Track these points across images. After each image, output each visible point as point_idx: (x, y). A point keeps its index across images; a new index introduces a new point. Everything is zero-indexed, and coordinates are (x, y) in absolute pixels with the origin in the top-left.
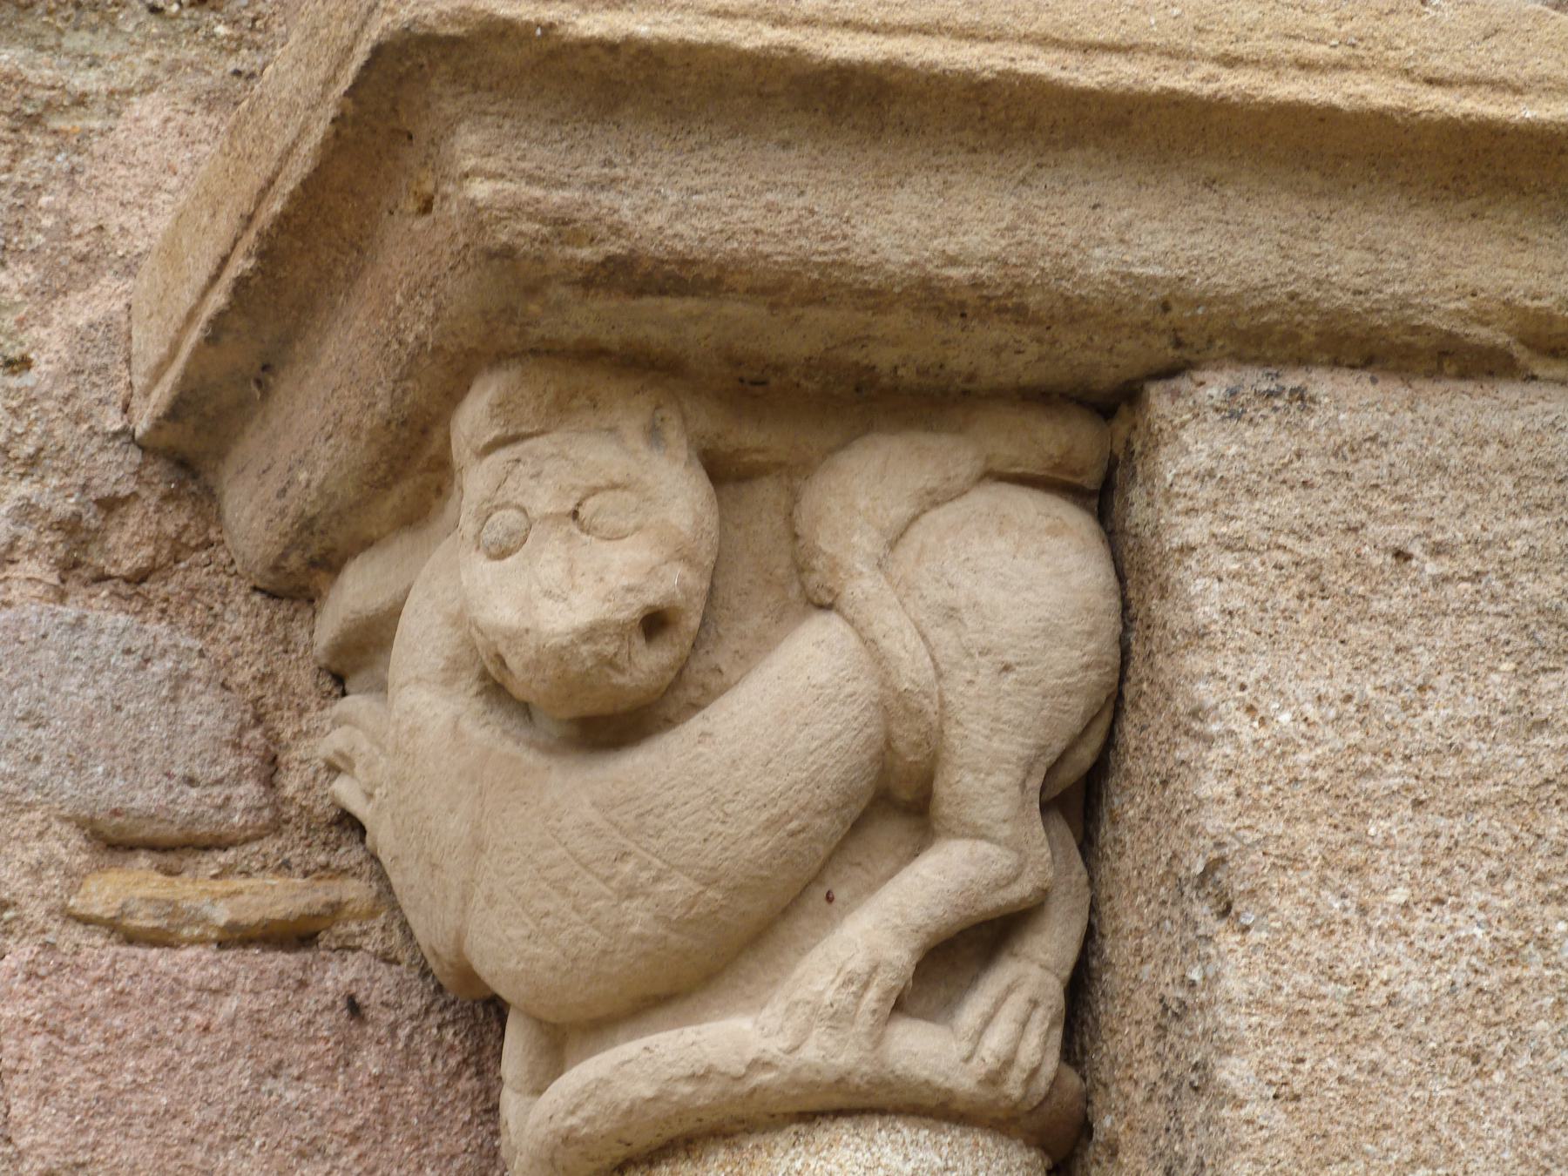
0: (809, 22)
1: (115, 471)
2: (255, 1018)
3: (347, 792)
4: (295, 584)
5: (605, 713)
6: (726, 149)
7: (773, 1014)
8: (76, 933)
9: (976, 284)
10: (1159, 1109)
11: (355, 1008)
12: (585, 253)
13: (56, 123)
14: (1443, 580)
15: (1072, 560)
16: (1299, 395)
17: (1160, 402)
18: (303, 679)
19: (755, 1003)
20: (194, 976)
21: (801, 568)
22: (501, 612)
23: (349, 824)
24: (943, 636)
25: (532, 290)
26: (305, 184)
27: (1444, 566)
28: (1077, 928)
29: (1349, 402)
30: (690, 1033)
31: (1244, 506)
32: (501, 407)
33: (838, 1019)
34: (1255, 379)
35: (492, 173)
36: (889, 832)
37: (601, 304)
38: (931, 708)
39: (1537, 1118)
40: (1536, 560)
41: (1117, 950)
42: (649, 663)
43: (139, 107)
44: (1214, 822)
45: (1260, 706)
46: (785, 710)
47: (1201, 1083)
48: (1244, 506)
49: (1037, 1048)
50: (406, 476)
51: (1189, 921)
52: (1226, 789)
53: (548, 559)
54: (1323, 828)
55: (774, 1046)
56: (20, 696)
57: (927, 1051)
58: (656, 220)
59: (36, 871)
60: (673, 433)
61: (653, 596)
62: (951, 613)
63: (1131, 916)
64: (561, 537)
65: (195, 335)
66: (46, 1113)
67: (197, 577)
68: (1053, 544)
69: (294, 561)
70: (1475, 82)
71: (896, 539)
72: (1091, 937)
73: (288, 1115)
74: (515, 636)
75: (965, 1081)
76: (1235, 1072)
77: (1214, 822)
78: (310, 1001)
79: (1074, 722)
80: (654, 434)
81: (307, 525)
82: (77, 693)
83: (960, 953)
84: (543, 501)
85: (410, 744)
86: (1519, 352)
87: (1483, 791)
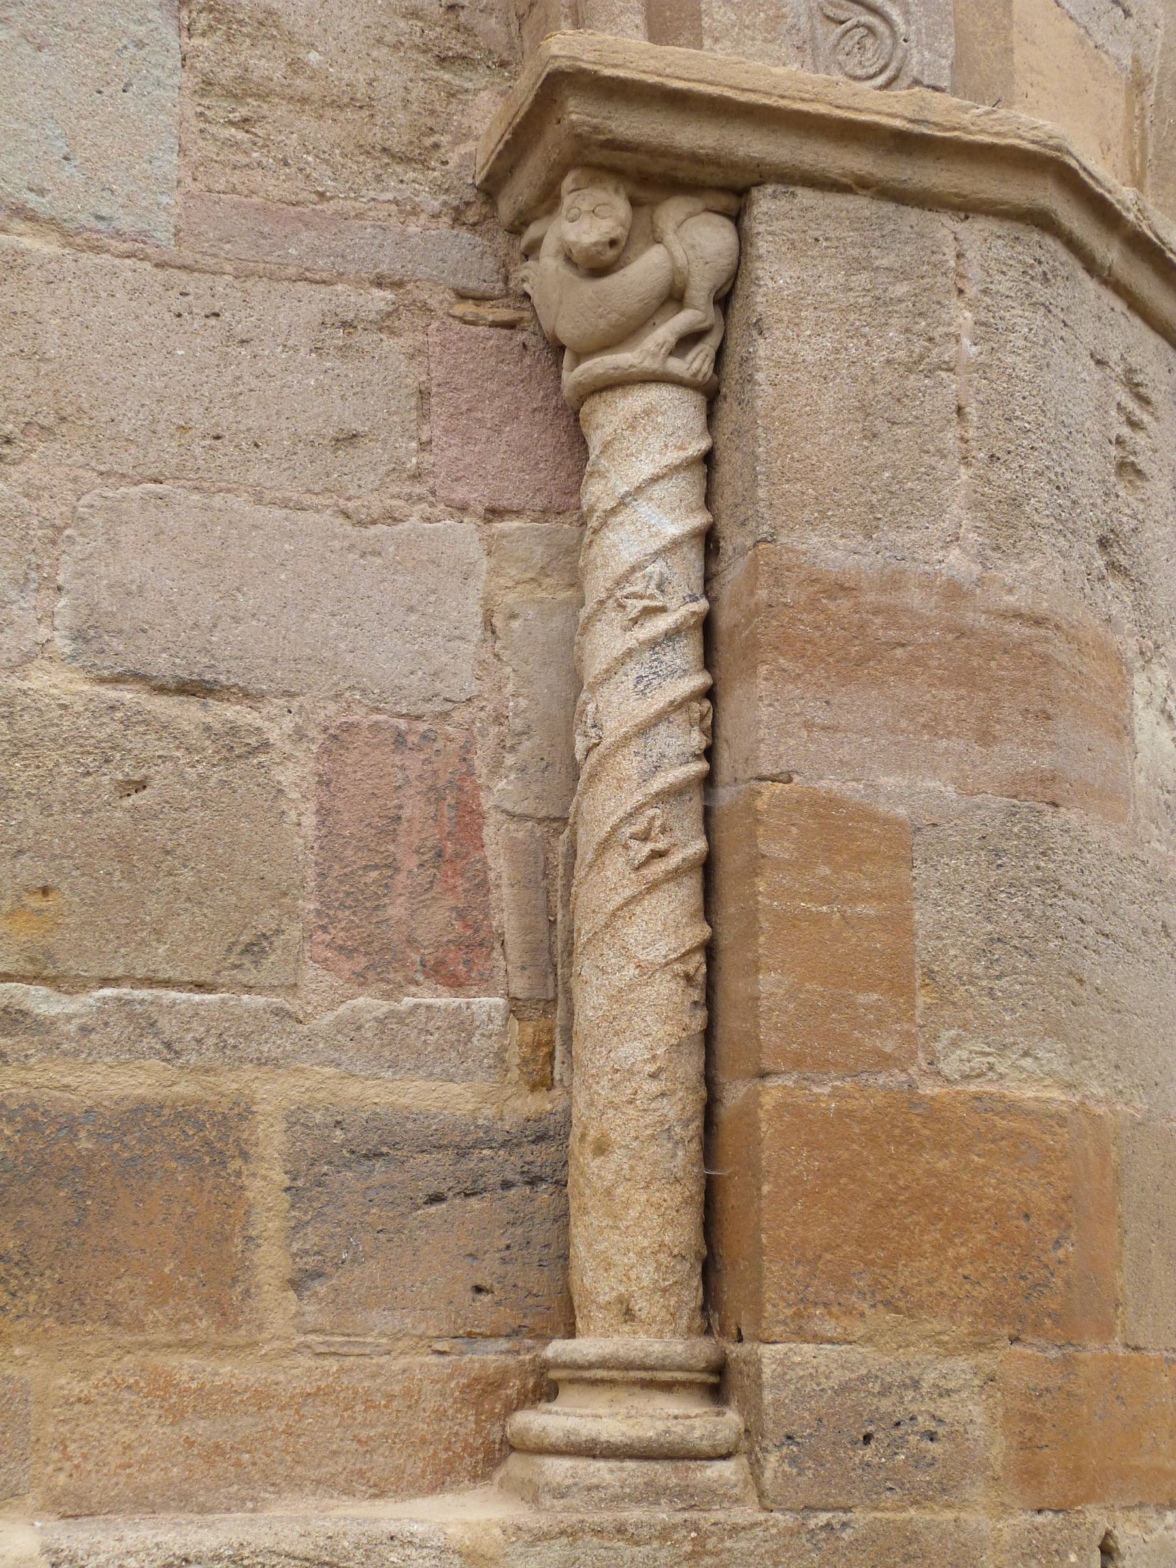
0: (667, 76)
1: (470, 194)
2: (497, 346)
3: (526, 287)
4: (516, 229)
5: (597, 266)
6: (642, 111)
7: (636, 353)
8: (451, 320)
9: (707, 155)
10: (739, 387)
11: (524, 346)
12: (601, 137)
13: (459, 96)
14: (827, 248)
15: (727, 235)
16: (793, 193)
17: (755, 192)
18: (517, 256)
19: (632, 350)
20: (482, 334)
21: (653, 231)
22: (571, 237)
23: (527, 296)
24: (690, 252)
25: (586, 146)
26: (526, 114)
27: (829, 244)
28: (720, 337)
29: (806, 196)
30: (614, 356)
31: (775, 223)
32: (576, 180)
33: (655, 355)
34: (781, 188)
35: (577, 112)
36: (672, 306)
37: (605, 152)
38: (686, 272)
39: (840, 396)
40: (853, 244)
41: (730, 343)
42: (611, 254)
43: (482, 94)
44: (760, 308)
45: (775, 278)
46: (646, 270)
47: (750, 380)
48: (775, 223)
49: (707, 368)
50: (548, 200)
51: (750, 335)
52: (764, 300)
53: (585, 223)
54: (789, 313)
55: (636, 362)
56: (440, 254)
57: (677, 366)
58: (621, 129)
59: (441, 302)
60: (622, 190)
61: (612, 236)
62: (693, 247)
63: (735, 334)
64: (589, 217)
65: (494, 157)
66: (440, 368)
67: (490, 225)
68: (722, 230)
69: (516, 223)
70: (849, 108)
71: (680, 225)
72: (724, 340)
73: (505, 373)
74: (574, 244)
75: (687, 375)
76: (760, 377)
77: (760, 308)
78: (513, 343)
79: (724, 279)
80: (617, 191)
81: (521, 213)
82: (455, 254)
83: (687, 341)
84: (585, 207)
85: (545, 274)
86: (853, 186)
87: (833, 306)
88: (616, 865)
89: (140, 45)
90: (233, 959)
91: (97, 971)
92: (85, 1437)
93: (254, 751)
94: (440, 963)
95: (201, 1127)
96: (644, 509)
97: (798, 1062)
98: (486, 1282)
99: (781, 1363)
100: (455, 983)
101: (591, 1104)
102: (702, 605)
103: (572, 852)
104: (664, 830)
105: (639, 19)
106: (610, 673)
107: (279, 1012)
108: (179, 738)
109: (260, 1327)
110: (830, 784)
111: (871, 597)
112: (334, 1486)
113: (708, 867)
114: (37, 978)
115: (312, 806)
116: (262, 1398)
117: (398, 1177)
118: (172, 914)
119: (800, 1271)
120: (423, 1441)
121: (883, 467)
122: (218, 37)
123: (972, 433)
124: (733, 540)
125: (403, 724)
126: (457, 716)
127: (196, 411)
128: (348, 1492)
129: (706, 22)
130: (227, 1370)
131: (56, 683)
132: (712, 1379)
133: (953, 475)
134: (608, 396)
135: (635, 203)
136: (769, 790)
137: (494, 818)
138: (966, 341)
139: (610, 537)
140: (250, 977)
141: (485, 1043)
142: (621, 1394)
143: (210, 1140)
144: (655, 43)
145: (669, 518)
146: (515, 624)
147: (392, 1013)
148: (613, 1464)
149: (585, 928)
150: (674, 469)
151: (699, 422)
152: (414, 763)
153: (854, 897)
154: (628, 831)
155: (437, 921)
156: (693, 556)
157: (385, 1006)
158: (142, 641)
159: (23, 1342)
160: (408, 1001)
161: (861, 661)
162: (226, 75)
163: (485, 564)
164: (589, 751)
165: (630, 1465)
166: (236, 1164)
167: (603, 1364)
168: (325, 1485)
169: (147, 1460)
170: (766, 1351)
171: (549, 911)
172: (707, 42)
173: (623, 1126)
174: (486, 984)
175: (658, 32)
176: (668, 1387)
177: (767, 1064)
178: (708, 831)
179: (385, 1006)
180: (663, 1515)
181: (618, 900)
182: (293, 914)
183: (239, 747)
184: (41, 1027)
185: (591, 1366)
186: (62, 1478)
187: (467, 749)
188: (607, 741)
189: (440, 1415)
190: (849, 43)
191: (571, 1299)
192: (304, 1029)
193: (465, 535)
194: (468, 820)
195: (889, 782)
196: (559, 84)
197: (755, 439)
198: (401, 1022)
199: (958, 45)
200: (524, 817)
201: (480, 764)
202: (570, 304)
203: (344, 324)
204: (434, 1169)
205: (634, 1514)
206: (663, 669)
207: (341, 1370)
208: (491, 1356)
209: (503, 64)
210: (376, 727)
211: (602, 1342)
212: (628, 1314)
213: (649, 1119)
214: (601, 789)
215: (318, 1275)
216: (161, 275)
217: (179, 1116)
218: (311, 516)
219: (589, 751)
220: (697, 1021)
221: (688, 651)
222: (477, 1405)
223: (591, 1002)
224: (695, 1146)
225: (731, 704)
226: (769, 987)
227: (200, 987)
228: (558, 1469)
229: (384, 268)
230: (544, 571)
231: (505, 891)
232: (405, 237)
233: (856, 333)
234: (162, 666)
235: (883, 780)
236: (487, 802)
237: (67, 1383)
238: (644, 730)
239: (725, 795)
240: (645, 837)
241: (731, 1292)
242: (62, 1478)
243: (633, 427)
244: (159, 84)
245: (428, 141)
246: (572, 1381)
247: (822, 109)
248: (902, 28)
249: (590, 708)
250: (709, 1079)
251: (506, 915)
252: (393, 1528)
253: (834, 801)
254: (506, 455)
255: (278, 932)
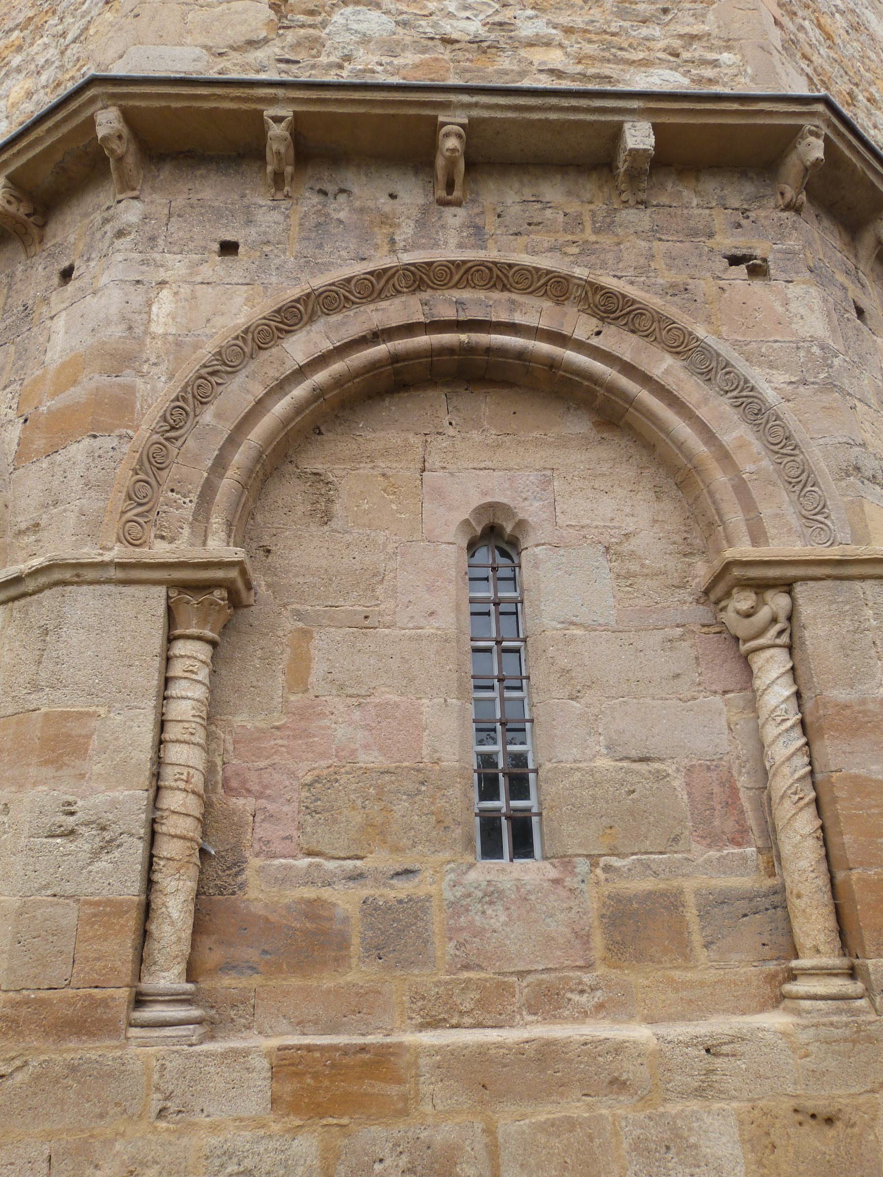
1: (700, 594)
4: (717, 603)
29: (811, 584)
41: (794, 631)
42: (752, 610)
45: (806, 611)
46: (764, 613)
50: (728, 595)
53: (743, 603)
57: (778, 641)
63: (795, 629)
76: (807, 643)
83: (780, 633)
85: (729, 617)
88: (787, 804)
89: (598, 568)
90: (669, 843)
91: (630, 851)
92: (650, 998)
93: (665, 777)
94: (733, 838)
95: (669, 898)
96: (776, 688)
97: (861, 864)
98: (766, 942)
99: (875, 965)
100: (739, 845)
101: (792, 882)
102: (799, 716)
103: (770, 799)
104: (801, 790)
105: (748, 538)
106: (774, 742)
107: (686, 859)
108: (642, 775)
109: (697, 961)
110: (854, 771)
111: (857, 708)
112: (729, 1012)
113: (817, 801)
114: (613, 855)
115: (685, 792)
116: (702, 984)
117: (732, 909)
118: (649, 831)
119: (875, 934)
120: (755, 996)
121: (853, 665)
122: (619, 561)
123: (879, 650)
124: (806, 694)
125: (708, 763)
126: (725, 758)
127: (631, 674)
128: (734, 1013)
129: (769, 535)
130: (689, 975)
131: (604, 763)
132: (850, 972)
133: (876, 664)
134: (757, 653)
135: (756, 594)
136: (835, 775)
137: (742, 790)
138: (872, 620)
139: (766, 697)
140: (676, 848)
141: (752, 863)
142: (821, 978)
143: (671, 902)
144: (757, 546)
145: (784, 690)
146: (738, 727)
147: (721, 856)
148: (824, 1002)
149: (780, 824)
150: (783, 674)
151: (788, 657)
152: (714, 775)
153: (869, 808)
154: (790, 792)
155: (730, 825)
156: (794, 700)
157: (718, 854)
158: (626, 747)
159: (627, 969)
160: (725, 852)
161: (858, 729)
162: (623, 572)
163: (725, 709)
164: (771, 767)
165: (830, 1002)
166: (681, 909)
167: (813, 968)
168: (726, 1011)
169: (670, 1005)
170: (869, 962)
171: (765, 818)
172: (770, 541)
173: (805, 889)
174: (749, 844)
175: (755, 542)
176: (836, 975)
177: (851, 865)
178: (815, 788)
179: (718, 854)
180: (844, 1018)
181: (790, 815)
182: (685, 827)
183: (660, 776)
184: (616, 870)
185: (809, 969)
186: (646, 1011)
187: (730, 768)
188: (777, 763)
189: (759, 987)
190: (815, 534)
191: (795, 946)
192: (695, 864)
193: (717, 701)
194: (734, 791)
195: (874, 768)
196: (729, 565)
197: (809, 662)
198: (724, 858)
199: (852, 530)
200: (751, 789)
201: (735, 774)
202: (741, 627)
203: (670, 641)
204: (743, 906)
205: (835, 1019)
206: (791, 738)
207: (725, 973)
208: (772, 967)
209: (703, 553)
210: (700, 765)
211: (811, 961)
212: (818, 951)
213: (813, 886)
214: (778, 779)
215: (712, 943)
216: (614, 635)
217: (661, 894)
218: (669, 701)
219: (771, 767)
220: (823, 852)
221: (798, 731)
222: (770, 983)
223: (786, 849)
224: (830, 893)
225: (816, 746)
226: (848, 840)
227: (661, 853)
228: (806, 1004)
229: (678, 622)
230: (744, 709)
231: (750, 813)
232: (683, 611)
233: (836, 624)
234: (634, 754)
235: (872, 767)
236: (739, 785)
237: (643, 982)
238: (789, 758)
239: (819, 777)
240: (795, 793)
241: (851, 942)
242: (646, 1011)
243: (767, 662)
244: (604, 578)
245: (685, 581)
246: (802, 974)
247: (813, 558)
248: (832, 527)
249: (769, 753)
250: (830, 871)
251: (751, 821)
252: (758, 1025)
253: (857, 776)
254: (726, 673)
255: (682, 833)
